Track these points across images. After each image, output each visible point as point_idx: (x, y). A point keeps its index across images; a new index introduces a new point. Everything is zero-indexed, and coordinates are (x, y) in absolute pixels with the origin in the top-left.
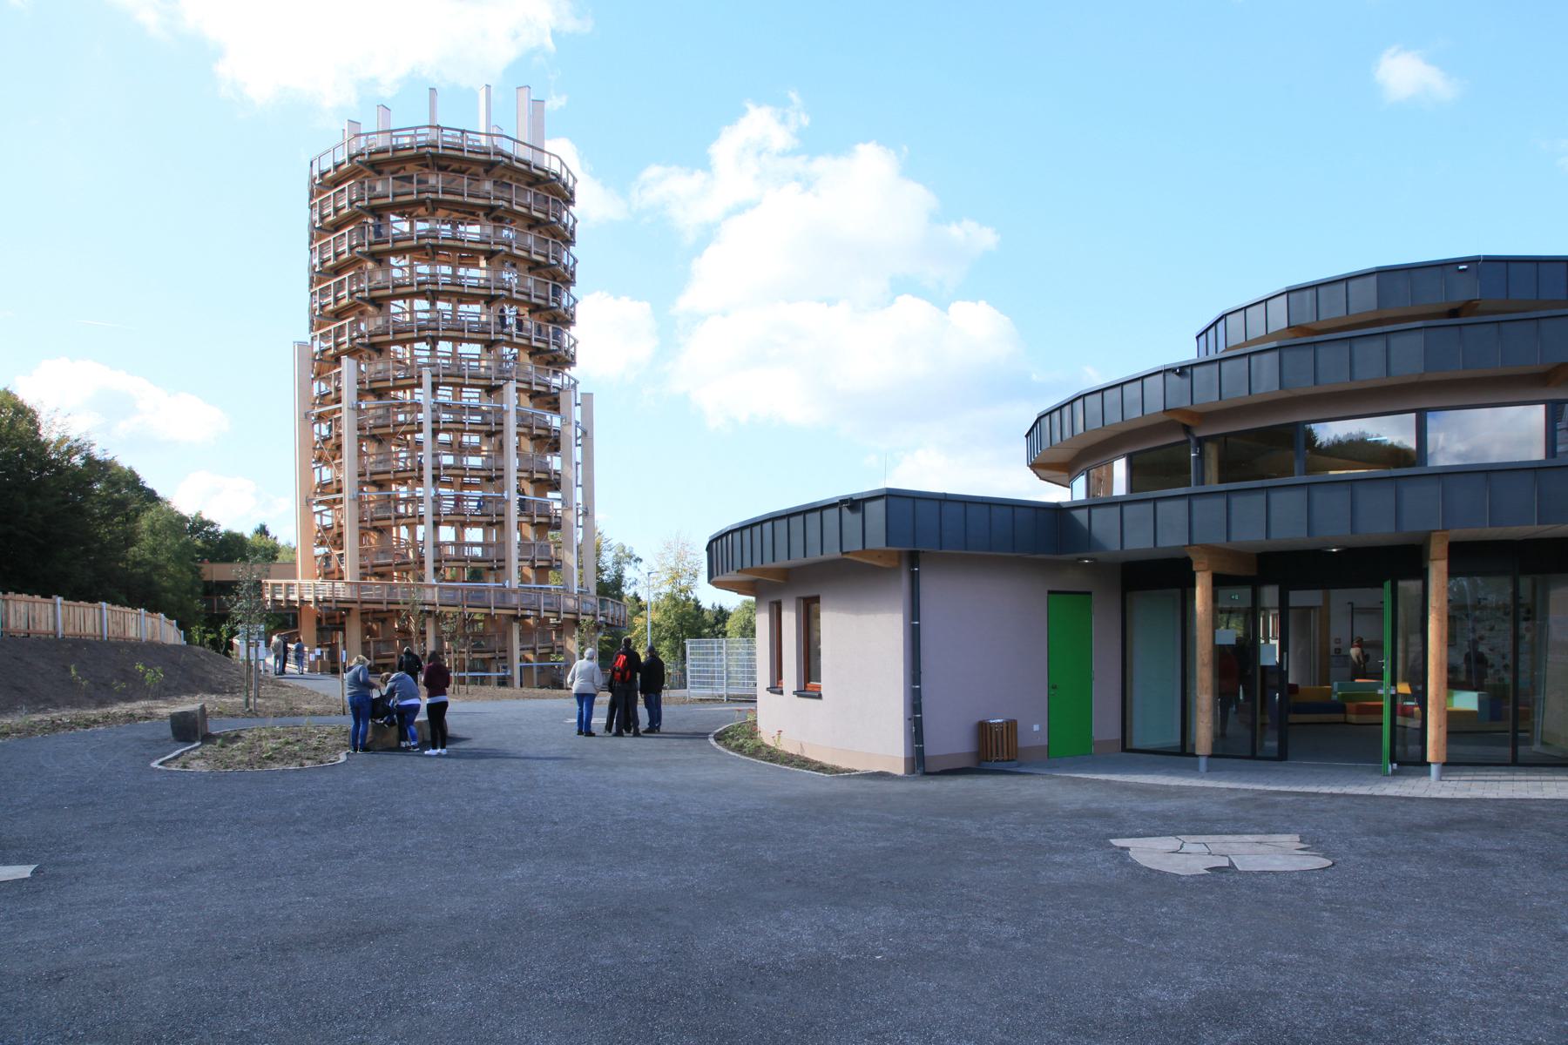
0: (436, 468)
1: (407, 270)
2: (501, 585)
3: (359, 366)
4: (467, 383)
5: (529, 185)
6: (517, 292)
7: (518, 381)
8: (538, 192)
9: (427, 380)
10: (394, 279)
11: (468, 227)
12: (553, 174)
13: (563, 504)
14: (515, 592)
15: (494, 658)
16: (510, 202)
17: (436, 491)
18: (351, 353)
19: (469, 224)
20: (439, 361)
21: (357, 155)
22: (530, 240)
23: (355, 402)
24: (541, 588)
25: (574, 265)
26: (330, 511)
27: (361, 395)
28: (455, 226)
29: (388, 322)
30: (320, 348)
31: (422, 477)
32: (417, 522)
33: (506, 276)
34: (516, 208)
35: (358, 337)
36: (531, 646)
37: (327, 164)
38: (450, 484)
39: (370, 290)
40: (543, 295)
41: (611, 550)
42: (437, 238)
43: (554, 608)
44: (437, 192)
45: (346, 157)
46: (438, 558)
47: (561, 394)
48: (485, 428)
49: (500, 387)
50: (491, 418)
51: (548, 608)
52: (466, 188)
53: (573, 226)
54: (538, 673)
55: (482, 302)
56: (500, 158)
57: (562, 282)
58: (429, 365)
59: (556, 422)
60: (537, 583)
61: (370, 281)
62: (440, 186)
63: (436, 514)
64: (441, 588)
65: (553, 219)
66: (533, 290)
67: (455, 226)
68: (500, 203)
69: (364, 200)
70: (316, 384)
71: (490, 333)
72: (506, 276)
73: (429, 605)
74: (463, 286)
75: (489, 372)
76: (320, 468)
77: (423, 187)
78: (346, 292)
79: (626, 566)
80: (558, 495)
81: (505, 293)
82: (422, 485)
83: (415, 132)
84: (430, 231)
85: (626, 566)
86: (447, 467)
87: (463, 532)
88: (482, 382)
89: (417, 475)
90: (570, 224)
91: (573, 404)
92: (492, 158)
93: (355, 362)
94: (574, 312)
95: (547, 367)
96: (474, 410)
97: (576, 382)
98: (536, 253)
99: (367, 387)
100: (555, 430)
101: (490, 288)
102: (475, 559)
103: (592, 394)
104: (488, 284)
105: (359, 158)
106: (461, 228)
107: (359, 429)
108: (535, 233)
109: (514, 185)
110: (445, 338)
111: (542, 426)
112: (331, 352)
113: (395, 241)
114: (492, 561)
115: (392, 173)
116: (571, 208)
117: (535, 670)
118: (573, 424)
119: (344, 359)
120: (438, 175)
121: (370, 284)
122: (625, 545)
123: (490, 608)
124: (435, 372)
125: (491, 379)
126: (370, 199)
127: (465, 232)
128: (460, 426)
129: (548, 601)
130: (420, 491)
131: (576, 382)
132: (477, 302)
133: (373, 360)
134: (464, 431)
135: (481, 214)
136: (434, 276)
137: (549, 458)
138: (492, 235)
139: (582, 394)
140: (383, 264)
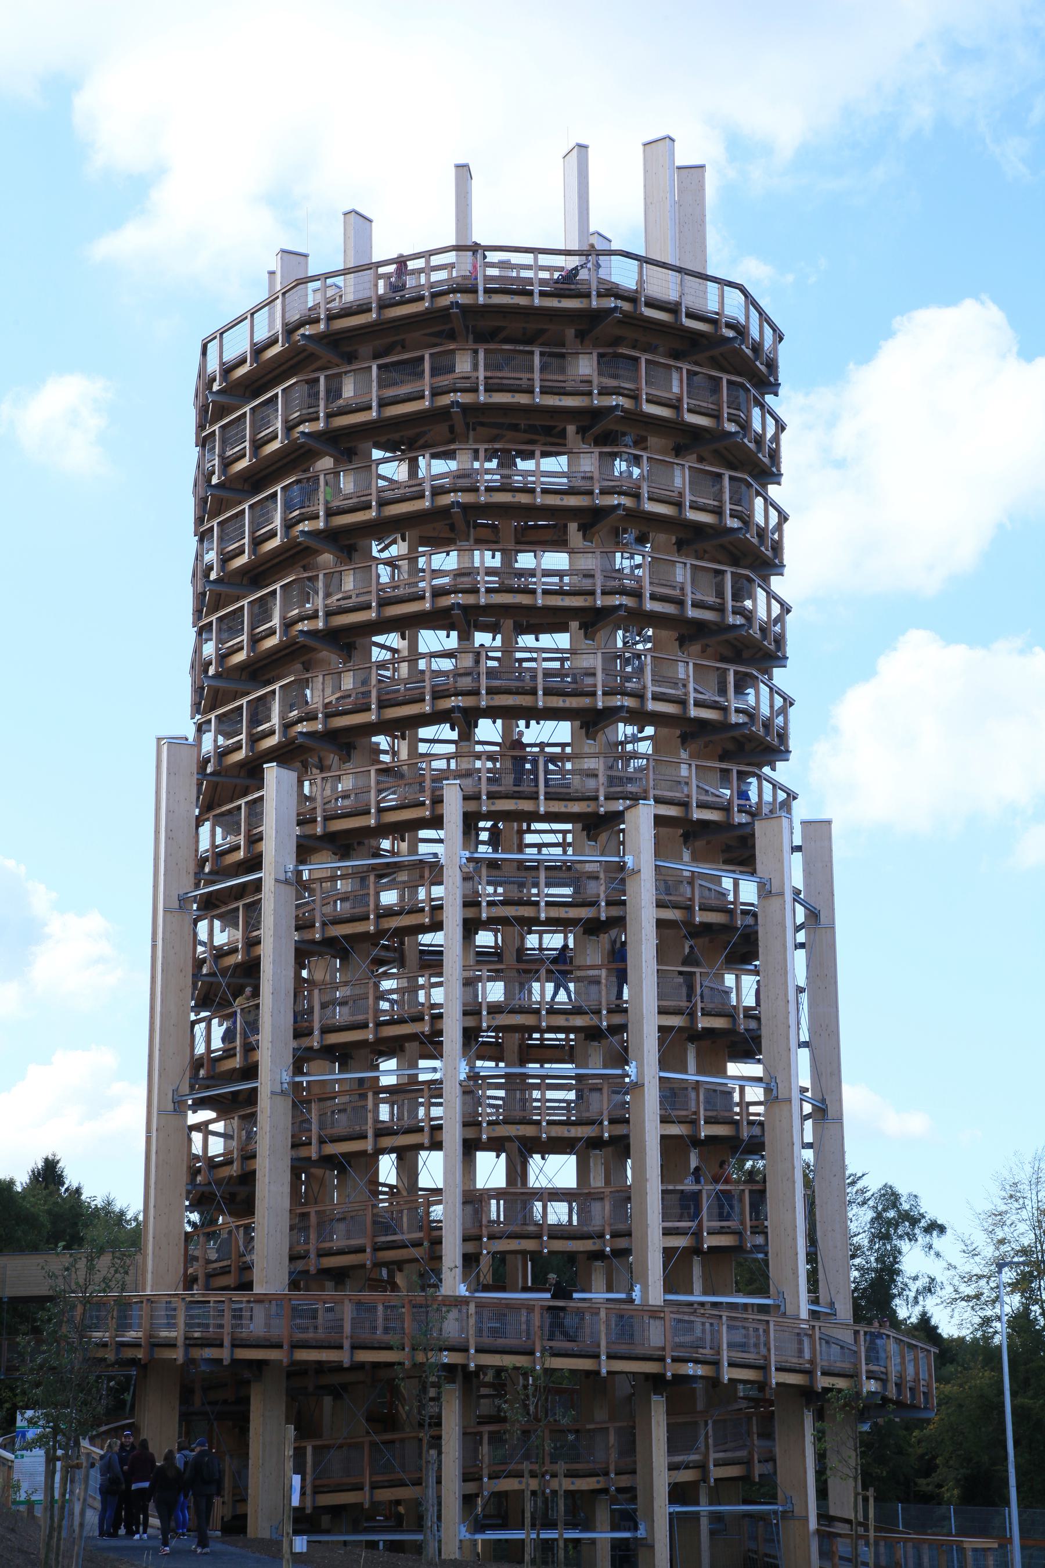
0: (472, 1011)
1: (404, 564)
2: (623, 1296)
3: (300, 783)
4: (542, 810)
5: (676, 355)
6: (653, 597)
7: (658, 801)
8: (697, 369)
9: (453, 808)
10: (381, 588)
11: (543, 461)
12: (729, 326)
13: (768, 1091)
14: (655, 1313)
15: (605, 1491)
16: (635, 397)
17: (472, 1067)
18: (284, 755)
19: (545, 454)
20: (478, 764)
21: (301, 324)
22: (680, 479)
23: (291, 867)
24: (715, 1305)
25: (779, 528)
26: (222, 1123)
27: (305, 850)
28: (507, 462)
29: (365, 682)
30: (217, 747)
31: (440, 1033)
32: (426, 1142)
33: (621, 561)
34: (649, 409)
35: (300, 720)
36: (694, 1457)
37: (237, 345)
38: (495, 1052)
39: (328, 614)
40: (711, 599)
41: (864, 1203)
42: (476, 490)
43: (750, 1357)
44: (475, 390)
45: (278, 326)
46: (474, 1231)
47: (758, 825)
48: (584, 913)
49: (618, 816)
50: (599, 890)
51: (738, 1356)
52: (537, 376)
53: (776, 438)
54: (712, 1533)
55: (574, 625)
56: (611, 303)
57: (751, 567)
58: (459, 775)
59: (748, 892)
60: (705, 1293)
61: (328, 595)
62: (481, 374)
63: (470, 1123)
64: (480, 1305)
65: (732, 427)
66: (688, 589)
67: (507, 462)
68: (614, 401)
69: (317, 419)
70: (205, 830)
71: (593, 694)
72: (621, 561)
73: (451, 1349)
74: (533, 592)
75: (591, 783)
76: (208, 1021)
77: (444, 381)
78: (276, 621)
79: (905, 1246)
80: (755, 1070)
81: (625, 600)
82: (437, 1055)
83: (428, 262)
84: (460, 475)
85: (905, 1246)
86: (495, 1009)
87: (525, 1165)
88: (576, 808)
89: (427, 1029)
90: (770, 432)
91: (787, 848)
92: (595, 303)
93: (293, 775)
94: (785, 727)
95: (724, 766)
96: (560, 873)
97: (792, 796)
98: (694, 507)
99: (319, 830)
100: (745, 913)
101: (592, 593)
102: (558, 1233)
103: (829, 822)
104: (586, 584)
105: (307, 330)
106: (522, 465)
107: (298, 928)
108: (690, 461)
109: (644, 358)
110: (492, 713)
111: (714, 902)
112: (241, 755)
113: (382, 503)
114: (601, 1236)
115: (376, 357)
116: (773, 490)
117: (704, 1522)
118: (789, 896)
119: (272, 772)
120: (476, 352)
121: (329, 602)
122: (989, 1207)
123: (597, 1356)
124: (470, 790)
125: (596, 798)
126: (329, 416)
127: (538, 473)
128: (527, 912)
129: (738, 1338)
130: (428, 1069)
131: (792, 796)
132: (562, 628)
133: (329, 769)
134: (536, 921)
135: (571, 429)
136: (469, 574)
137: (730, 980)
138: (596, 475)
139: (803, 823)
140: (356, 556)
